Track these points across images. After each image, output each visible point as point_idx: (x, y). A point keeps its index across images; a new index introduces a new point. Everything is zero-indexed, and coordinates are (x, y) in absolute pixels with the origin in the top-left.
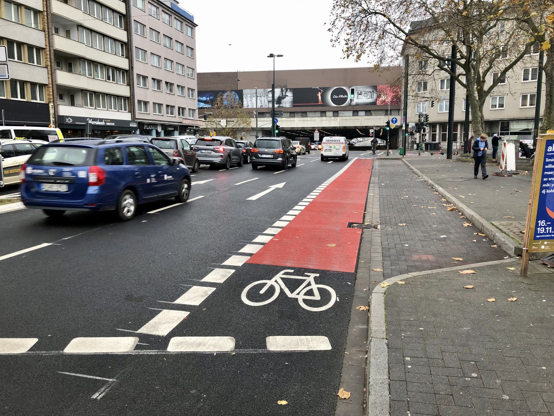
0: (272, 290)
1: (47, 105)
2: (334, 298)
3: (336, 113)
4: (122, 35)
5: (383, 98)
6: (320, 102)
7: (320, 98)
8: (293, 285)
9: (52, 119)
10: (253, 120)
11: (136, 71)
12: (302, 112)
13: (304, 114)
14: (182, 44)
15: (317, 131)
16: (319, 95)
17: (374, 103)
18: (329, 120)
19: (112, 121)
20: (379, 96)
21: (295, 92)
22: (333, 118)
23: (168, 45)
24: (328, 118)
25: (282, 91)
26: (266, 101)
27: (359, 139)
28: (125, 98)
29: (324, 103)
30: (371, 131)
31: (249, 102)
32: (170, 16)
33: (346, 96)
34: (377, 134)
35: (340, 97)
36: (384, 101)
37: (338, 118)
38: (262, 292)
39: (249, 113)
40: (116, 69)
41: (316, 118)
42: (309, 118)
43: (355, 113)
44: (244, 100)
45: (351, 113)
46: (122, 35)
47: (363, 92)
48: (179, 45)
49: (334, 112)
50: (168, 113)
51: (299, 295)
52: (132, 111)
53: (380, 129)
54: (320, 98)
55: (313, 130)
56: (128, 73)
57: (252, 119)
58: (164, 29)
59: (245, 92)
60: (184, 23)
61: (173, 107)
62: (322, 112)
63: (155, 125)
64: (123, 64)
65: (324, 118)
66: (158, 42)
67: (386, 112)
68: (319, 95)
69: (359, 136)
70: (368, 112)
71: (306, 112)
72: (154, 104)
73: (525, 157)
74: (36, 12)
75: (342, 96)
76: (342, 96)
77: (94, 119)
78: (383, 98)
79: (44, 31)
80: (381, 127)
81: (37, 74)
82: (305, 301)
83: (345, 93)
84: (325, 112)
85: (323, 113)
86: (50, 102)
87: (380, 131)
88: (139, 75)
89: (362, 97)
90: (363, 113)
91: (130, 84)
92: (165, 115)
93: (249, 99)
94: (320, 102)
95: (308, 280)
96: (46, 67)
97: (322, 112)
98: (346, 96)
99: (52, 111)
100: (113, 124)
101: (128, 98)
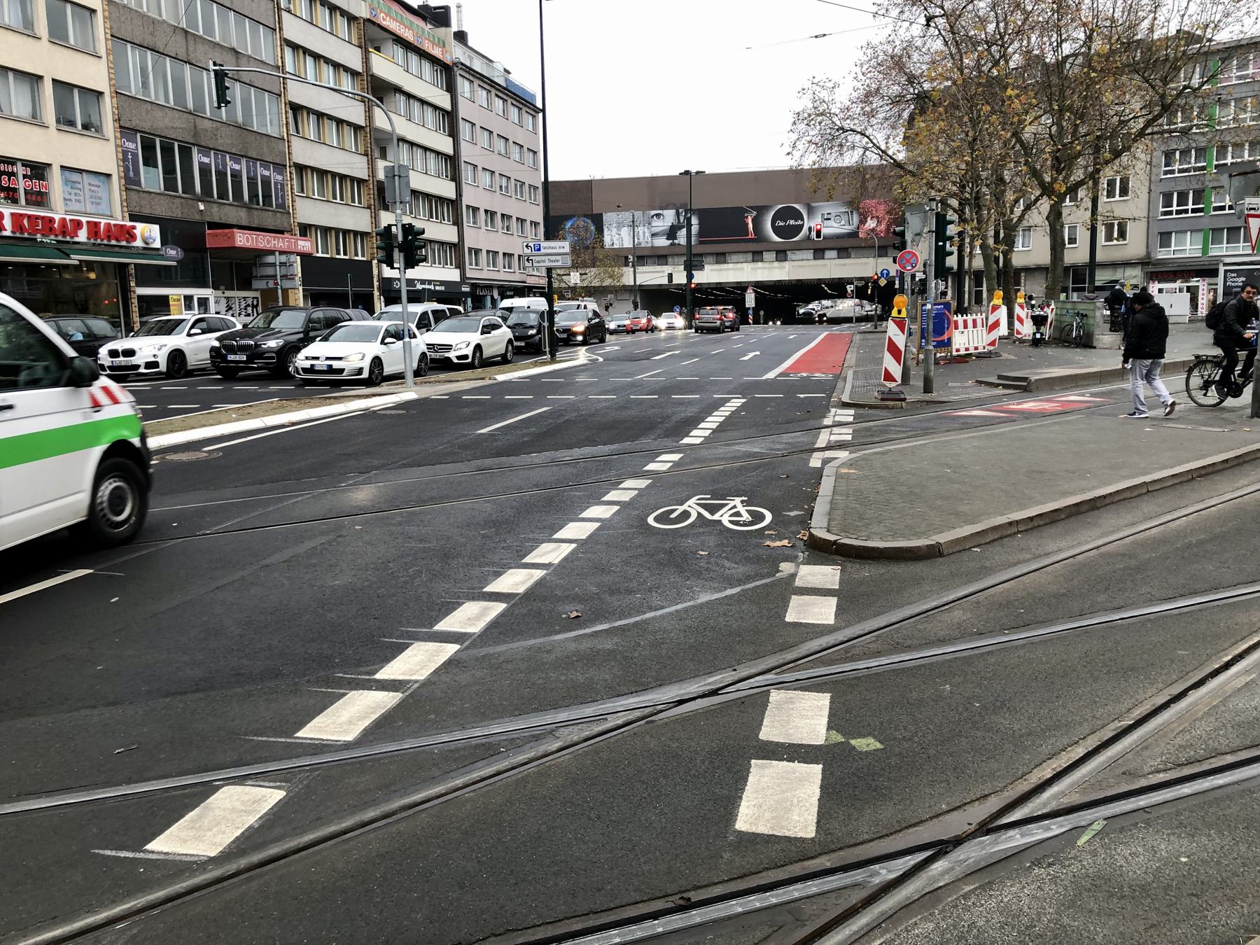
0: (686, 515)
1: (369, 263)
2: (769, 517)
3: (781, 255)
4: (446, 145)
5: (871, 224)
6: (752, 235)
7: (751, 226)
8: (713, 509)
9: (376, 284)
10: (628, 271)
11: (466, 201)
12: (717, 254)
13: (721, 258)
14: (522, 146)
15: (750, 291)
16: (750, 221)
17: (854, 235)
18: (770, 269)
19: (442, 283)
20: (863, 221)
21: (704, 214)
22: (776, 264)
23: (503, 152)
24: (767, 265)
25: (678, 214)
26: (647, 234)
27: (826, 303)
28: (452, 245)
29: (760, 237)
30: (850, 288)
31: (617, 236)
32: (505, 101)
33: (800, 222)
34: (861, 294)
35: (788, 223)
36: (873, 230)
37: (786, 264)
38: (673, 516)
39: (622, 258)
40: (441, 199)
41: (745, 265)
42: (731, 266)
43: (819, 253)
44: (606, 232)
45: (810, 254)
46: (446, 145)
47: (831, 216)
48: (517, 148)
49: (778, 252)
50: (488, 265)
51: (724, 517)
52: (460, 266)
53: (867, 284)
54: (751, 226)
55: (741, 287)
56: (453, 206)
57: (625, 269)
58: (498, 126)
59: (607, 217)
60: (525, 109)
61: (511, 255)
62: (754, 253)
63: (490, 287)
64: (446, 189)
65: (760, 264)
66: (507, 156)
67: (882, 251)
68: (750, 221)
69: (822, 296)
70: (844, 252)
71: (724, 254)
72: (488, 252)
73: (242, 239)
74: (357, 128)
75: (792, 222)
76: (792, 222)
77: (423, 282)
78: (871, 224)
79: (366, 155)
80: (867, 280)
81: (355, 218)
82: (731, 522)
83: (798, 216)
84: (761, 252)
85: (757, 256)
86: (373, 259)
87: (866, 287)
88: (468, 207)
89: (830, 220)
90: (834, 254)
91: (458, 222)
92: (486, 268)
93: (614, 230)
94: (752, 235)
95: (732, 504)
96: (369, 207)
97: (754, 253)
98: (800, 222)
99: (375, 272)
100: (443, 288)
101: (454, 245)
